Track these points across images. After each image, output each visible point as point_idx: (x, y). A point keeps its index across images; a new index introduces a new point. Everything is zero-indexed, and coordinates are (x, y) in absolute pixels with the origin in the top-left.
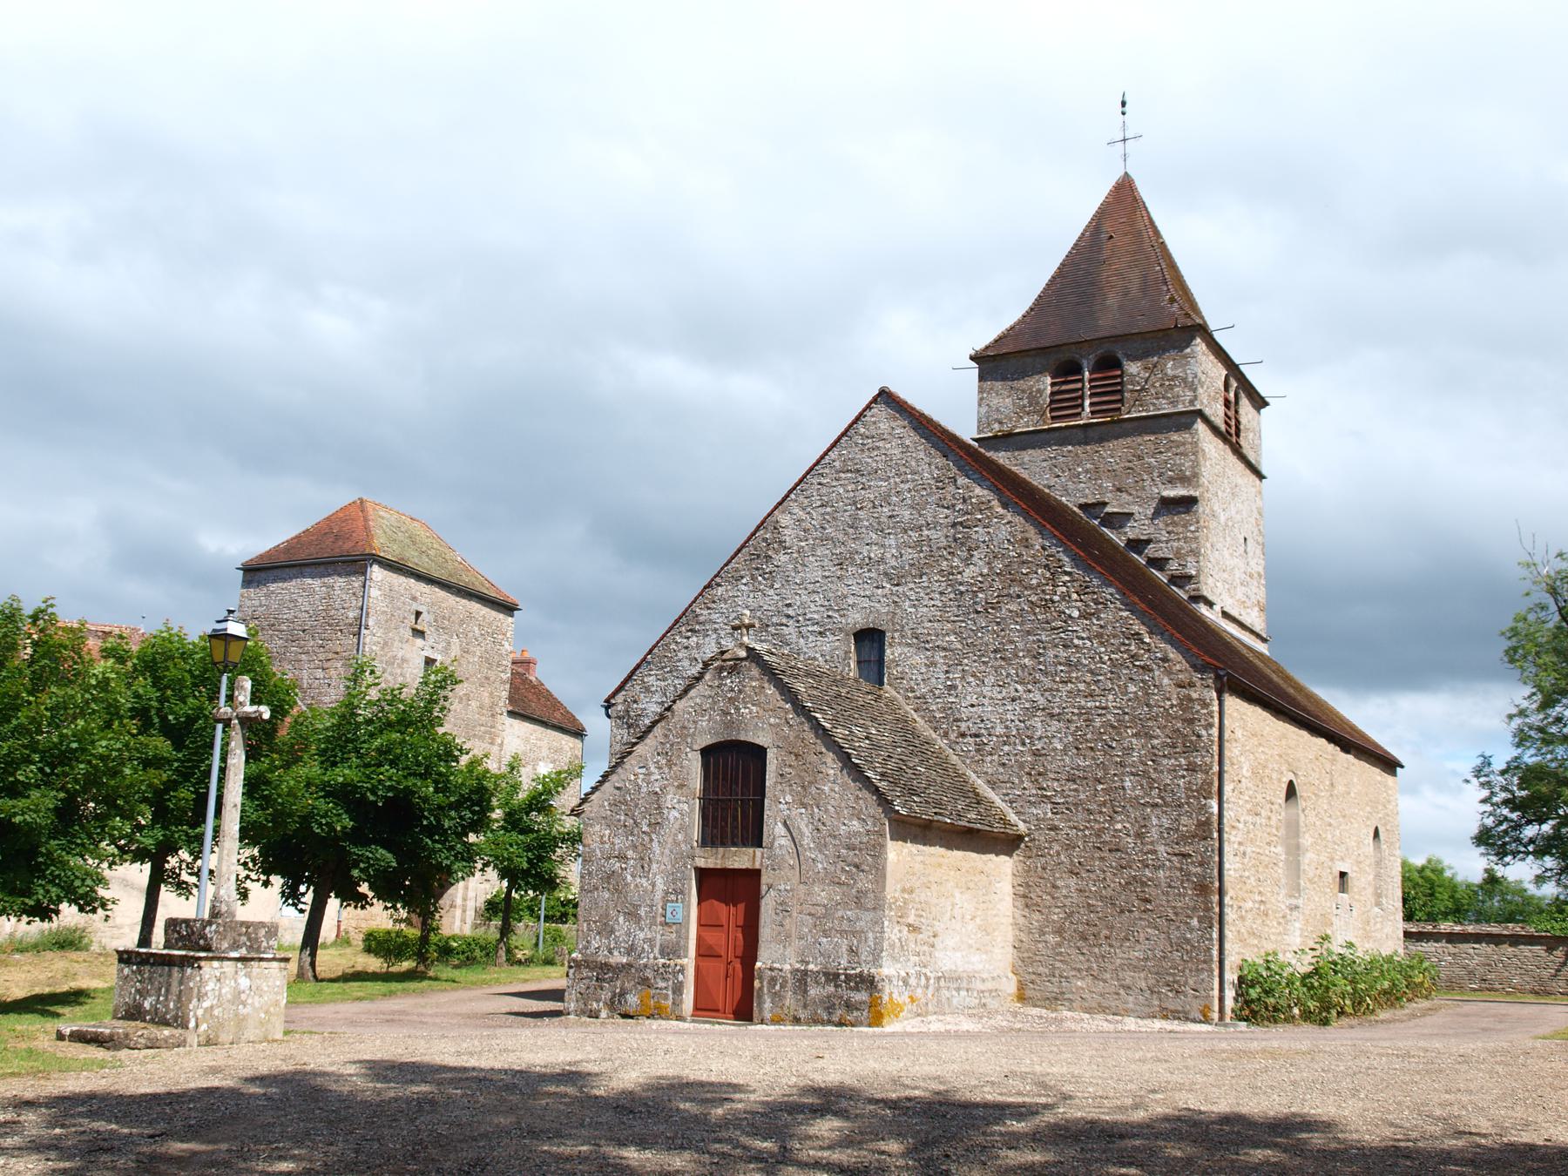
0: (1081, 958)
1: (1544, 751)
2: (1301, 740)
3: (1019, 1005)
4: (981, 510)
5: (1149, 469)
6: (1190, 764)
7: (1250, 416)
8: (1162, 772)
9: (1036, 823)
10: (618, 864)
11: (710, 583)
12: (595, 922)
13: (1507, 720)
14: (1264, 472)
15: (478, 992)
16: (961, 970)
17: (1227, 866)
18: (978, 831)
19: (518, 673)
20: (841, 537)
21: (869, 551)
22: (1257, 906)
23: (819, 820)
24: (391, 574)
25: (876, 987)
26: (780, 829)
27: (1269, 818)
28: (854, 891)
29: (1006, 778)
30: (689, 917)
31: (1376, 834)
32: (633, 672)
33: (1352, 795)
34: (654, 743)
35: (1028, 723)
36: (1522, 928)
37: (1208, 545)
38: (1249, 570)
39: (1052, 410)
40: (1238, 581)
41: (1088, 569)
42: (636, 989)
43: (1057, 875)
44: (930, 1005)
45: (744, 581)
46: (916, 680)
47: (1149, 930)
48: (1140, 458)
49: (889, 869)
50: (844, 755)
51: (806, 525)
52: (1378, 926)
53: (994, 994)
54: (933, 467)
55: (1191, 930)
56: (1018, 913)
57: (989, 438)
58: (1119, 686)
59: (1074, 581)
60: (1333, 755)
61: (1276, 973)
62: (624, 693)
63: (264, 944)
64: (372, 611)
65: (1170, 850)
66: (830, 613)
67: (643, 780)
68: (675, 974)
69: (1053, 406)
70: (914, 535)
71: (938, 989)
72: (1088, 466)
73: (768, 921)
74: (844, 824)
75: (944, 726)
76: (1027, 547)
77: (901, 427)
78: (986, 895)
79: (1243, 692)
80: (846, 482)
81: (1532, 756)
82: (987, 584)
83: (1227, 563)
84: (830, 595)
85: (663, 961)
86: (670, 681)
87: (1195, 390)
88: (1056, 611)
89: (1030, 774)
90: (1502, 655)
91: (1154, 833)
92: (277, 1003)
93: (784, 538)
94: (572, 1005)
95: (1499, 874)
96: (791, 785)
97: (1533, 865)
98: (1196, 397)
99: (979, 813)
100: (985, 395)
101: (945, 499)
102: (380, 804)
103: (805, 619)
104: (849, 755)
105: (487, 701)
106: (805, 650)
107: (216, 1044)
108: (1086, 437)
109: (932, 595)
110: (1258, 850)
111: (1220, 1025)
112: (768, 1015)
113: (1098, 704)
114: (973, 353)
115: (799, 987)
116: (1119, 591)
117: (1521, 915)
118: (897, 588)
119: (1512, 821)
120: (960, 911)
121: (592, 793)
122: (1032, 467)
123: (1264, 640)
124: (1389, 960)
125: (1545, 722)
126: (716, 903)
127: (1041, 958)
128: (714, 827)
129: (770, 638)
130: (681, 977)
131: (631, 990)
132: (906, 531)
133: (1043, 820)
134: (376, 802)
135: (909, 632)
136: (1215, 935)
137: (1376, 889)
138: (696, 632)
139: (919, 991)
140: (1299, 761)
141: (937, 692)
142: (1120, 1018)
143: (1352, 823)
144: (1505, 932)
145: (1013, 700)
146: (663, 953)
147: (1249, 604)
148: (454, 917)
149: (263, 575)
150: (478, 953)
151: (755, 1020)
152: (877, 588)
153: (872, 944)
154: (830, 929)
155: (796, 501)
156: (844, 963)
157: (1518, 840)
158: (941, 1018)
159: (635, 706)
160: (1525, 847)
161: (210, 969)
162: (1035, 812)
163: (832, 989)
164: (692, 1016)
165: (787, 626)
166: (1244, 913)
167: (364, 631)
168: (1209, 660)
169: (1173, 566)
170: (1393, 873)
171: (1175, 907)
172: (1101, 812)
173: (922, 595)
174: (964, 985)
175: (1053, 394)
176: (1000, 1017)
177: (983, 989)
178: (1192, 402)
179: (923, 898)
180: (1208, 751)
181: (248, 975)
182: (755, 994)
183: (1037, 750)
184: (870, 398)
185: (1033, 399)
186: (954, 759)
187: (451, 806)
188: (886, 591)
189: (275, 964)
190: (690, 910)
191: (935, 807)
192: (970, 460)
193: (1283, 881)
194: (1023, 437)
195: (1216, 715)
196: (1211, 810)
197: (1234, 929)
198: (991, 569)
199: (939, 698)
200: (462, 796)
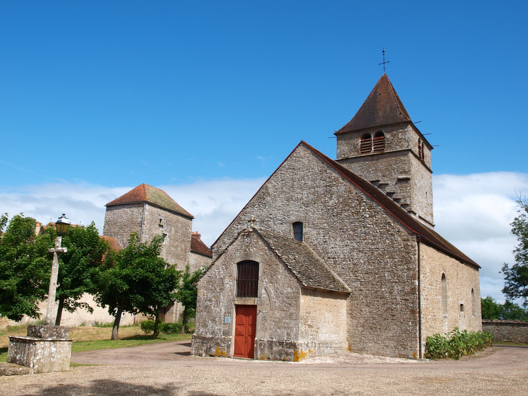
0: (371, 336)
1: (525, 262)
2: (447, 259)
3: (349, 352)
4: (335, 181)
6: (408, 268)
7: (427, 152)
8: (398, 271)
9: (354, 288)
10: (209, 303)
11: (245, 207)
12: (201, 323)
13: (513, 252)
14: (432, 171)
15: (171, 344)
16: (328, 340)
17: (421, 303)
18: (334, 291)
20: (288, 191)
22: (432, 317)
23: (277, 288)
24: (152, 207)
25: (296, 347)
26: (263, 291)
27: (436, 286)
28: (289, 313)
32: (220, 237)
33: (464, 278)
34: (221, 261)
35: (351, 254)
36: (521, 321)
37: (414, 194)
38: (428, 203)
39: (361, 150)
40: (424, 206)
41: (372, 200)
42: (215, 346)
44: (316, 353)
45: (256, 206)
46: (313, 239)
47: (394, 326)
48: (390, 165)
49: (301, 305)
52: (474, 322)
53: (340, 348)
54: (319, 167)
55: (409, 326)
56: (349, 320)
58: (383, 241)
62: (217, 244)
63: (63, 335)
64: (145, 219)
65: (401, 298)
66: (284, 217)
67: (218, 274)
68: (228, 341)
69: (362, 149)
70: (313, 190)
71: (319, 347)
73: (259, 323)
79: (426, 242)
80: (290, 172)
81: (521, 264)
82: (337, 206)
87: (408, 143)
88: (361, 215)
89: (352, 271)
90: (511, 231)
91: (396, 292)
93: (269, 192)
94: (193, 351)
96: (267, 276)
97: (522, 299)
98: (409, 145)
99: (334, 285)
104: (287, 265)
106: (276, 229)
107: (41, 373)
108: (372, 159)
112: (259, 357)
113: (375, 247)
116: (383, 208)
117: (517, 315)
118: (307, 208)
119: (515, 285)
122: (355, 169)
125: (526, 253)
126: (241, 316)
127: (357, 336)
128: (242, 289)
129: (265, 225)
130: (230, 343)
131: (213, 347)
132: (310, 189)
133: (357, 287)
135: (311, 223)
136: (418, 328)
137: (473, 309)
139: (312, 348)
140: (446, 266)
141: (320, 243)
142: (384, 357)
144: (515, 323)
146: (224, 334)
147: (428, 214)
148: (173, 317)
149: (112, 208)
150: (177, 329)
151: (255, 358)
152: (300, 208)
153: (295, 332)
155: (273, 179)
156: (285, 338)
157: (517, 291)
161: (41, 344)
163: (281, 348)
164: (234, 356)
165: (270, 221)
167: (143, 225)
169: (402, 201)
170: (478, 304)
171: (403, 318)
172: (377, 285)
173: (315, 210)
174: (329, 345)
175: (361, 145)
176: (341, 357)
177: (336, 347)
178: (407, 147)
181: (55, 347)
182: (255, 349)
184: (298, 144)
185: (355, 147)
186: (326, 266)
187: (162, 282)
188: (303, 209)
189: (66, 342)
190: (233, 319)
191: (318, 283)
192: (331, 164)
193: (441, 308)
195: (417, 251)
196: (415, 284)
198: (338, 201)
199: (321, 245)
200: (166, 278)
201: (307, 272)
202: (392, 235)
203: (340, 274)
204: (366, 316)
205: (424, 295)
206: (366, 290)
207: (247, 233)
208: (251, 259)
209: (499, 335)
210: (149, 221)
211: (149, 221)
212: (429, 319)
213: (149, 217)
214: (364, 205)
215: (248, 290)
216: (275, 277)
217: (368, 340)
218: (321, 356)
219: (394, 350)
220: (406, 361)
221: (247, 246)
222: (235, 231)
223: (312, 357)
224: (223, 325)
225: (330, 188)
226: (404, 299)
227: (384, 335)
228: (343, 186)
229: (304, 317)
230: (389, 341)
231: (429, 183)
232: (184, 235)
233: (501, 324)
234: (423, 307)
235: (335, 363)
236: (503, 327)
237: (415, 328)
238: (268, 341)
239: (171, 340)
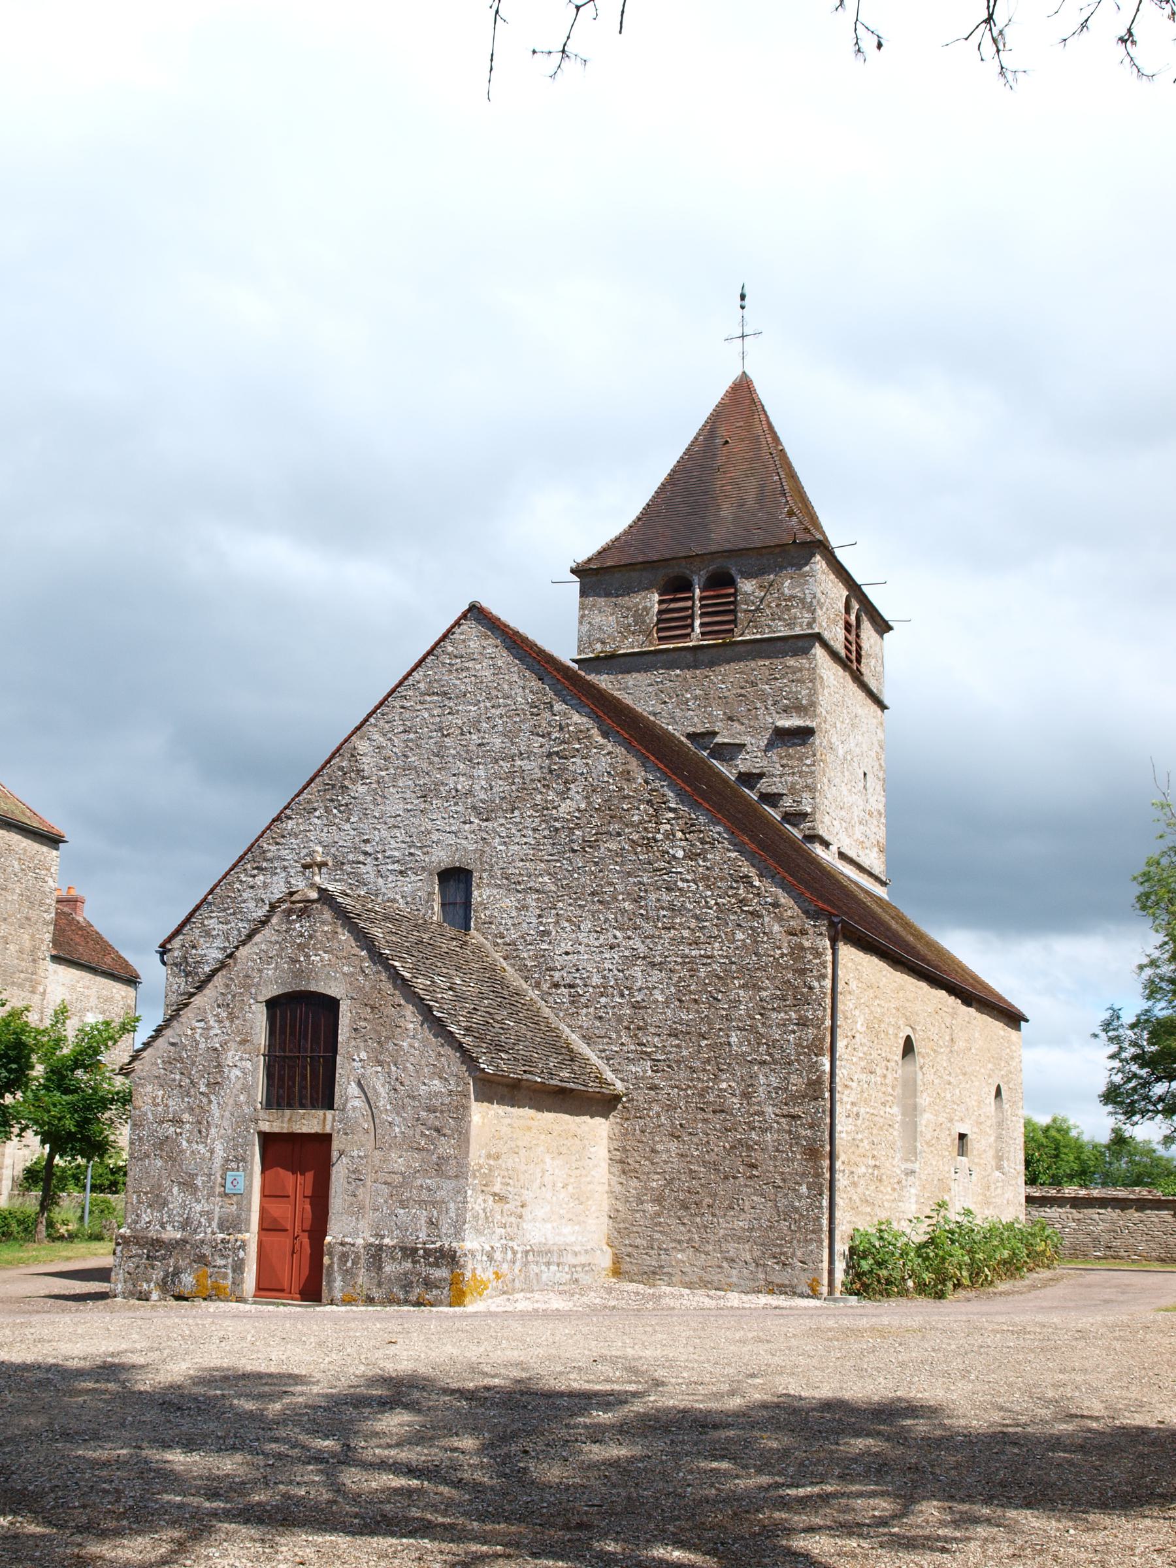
0: (682, 1228)
3: (614, 1280)
4: (579, 739)
5: (763, 697)
7: (872, 641)
8: (771, 1026)
9: (634, 1081)
10: (172, 1129)
12: (146, 1193)
14: (886, 702)
16: (551, 1242)
17: (838, 1128)
18: (572, 1090)
20: (425, 766)
22: (870, 1171)
23: (397, 1079)
25: (457, 1263)
26: (353, 1089)
27: (885, 1076)
28: (434, 1157)
29: (603, 1033)
30: (251, 1187)
32: (192, 915)
33: (973, 1051)
34: (214, 993)
36: (1150, 1192)
37: (825, 780)
38: (869, 807)
39: (659, 630)
40: (856, 819)
41: (694, 805)
42: (192, 1267)
43: (657, 1139)
45: (317, 814)
46: (506, 924)
47: (755, 1198)
48: (753, 684)
50: (425, 1008)
52: (999, 1191)
53: (587, 1268)
55: (800, 1197)
57: (590, 659)
59: (678, 818)
60: (953, 1008)
61: (889, 1243)
62: (181, 937)
65: (778, 1111)
66: (412, 850)
67: (201, 1034)
68: (235, 1250)
69: (660, 626)
70: (506, 765)
71: (526, 1264)
72: (698, 692)
74: (425, 1084)
75: (536, 975)
76: (629, 780)
77: (492, 646)
78: (580, 1160)
81: (1163, 1009)
83: (845, 800)
85: (222, 1236)
86: (233, 925)
87: (813, 612)
88: (658, 850)
89: (629, 1028)
91: (762, 1093)
93: (362, 766)
94: (120, 1286)
95: (1127, 1135)
96: (366, 1041)
98: (814, 620)
99: (573, 1072)
100: (586, 612)
101: (540, 727)
103: (385, 857)
104: (430, 1008)
105: (28, 944)
106: (384, 890)
110: (872, 1111)
111: (829, 1300)
112: (338, 1295)
113: (702, 952)
114: (574, 565)
116: (727, 830)
118: (486, 823)
119: (1141, 1078)
120: (551, 1177)
121: (143, 1050)
123: (883, 884)
126: (281, 1170)
128: (281, 1087)
129: (346, 877)
130: (241, 1254)
132: (497, 761)
133: (643, 1078)
135: (499, 872)
136: (825, 1203)
137: (997, 1151)
138: (262, 869)
139: (505, 1266)
140: (918, 1015)
141: (528, 938)
142: (723, 1293)
144: (1132, 1197)
147: (867, 844)
150: (15, 1228)
151: (324, 1300)
152: (464, 823)
153: (453, 1215)
155: (376, 726)
156: (423, 1236)
157: (1147, 1098)
158: (528, 1295)
159: (194, 951)
160: (1154, 1105)
163: (409, 1265)
164: (255, 1296)
165: (365, 864)
166: (856, 1179)
169: (787, 802)
170: (1016, 1135)
171: (782, 1173)
172: (704, 1070)
173: (513, 831)
174: (555, 1259)
175: (660, 612)
176: (592, 1294)
178: (810, 625)
179: (510, 1164)
184: (459, 614)
185: (639, 617)
186: (546, 1012)
188: (474, 827)
191: (524, 1065)
193: (899, 1144)
194: (628, 659)
195: (829, 965)
197: (845, 1196)
198: (589, 804)
201: (490, 1028)
202: (755, 914)
203: (591, 1038)
204: (668, 1168)
205: (847, 1103)
206: (672, 1087)
207: (301, 905)
212: (859, 1177)
214: (669, 820)
216: (390, 1046)
217: (675, 1241)
219: (754, 1270)
220: (789, 1303)
221: (299, 945)
222: (245, 895)
223: (504, 1293)
224: (218, 1199)
226: (787, 1116)
227: (723, 1226)
228: (604, 755)
229: (481, 1168)
230: (739, 1243)
231: (876, 744)
232: (29, 899)
233: (1089, 1202)
234: (841, 1139)
235: (575, 1309)
236: (1092, 1213)
237: (818, 1204)
239: (9, 1262)
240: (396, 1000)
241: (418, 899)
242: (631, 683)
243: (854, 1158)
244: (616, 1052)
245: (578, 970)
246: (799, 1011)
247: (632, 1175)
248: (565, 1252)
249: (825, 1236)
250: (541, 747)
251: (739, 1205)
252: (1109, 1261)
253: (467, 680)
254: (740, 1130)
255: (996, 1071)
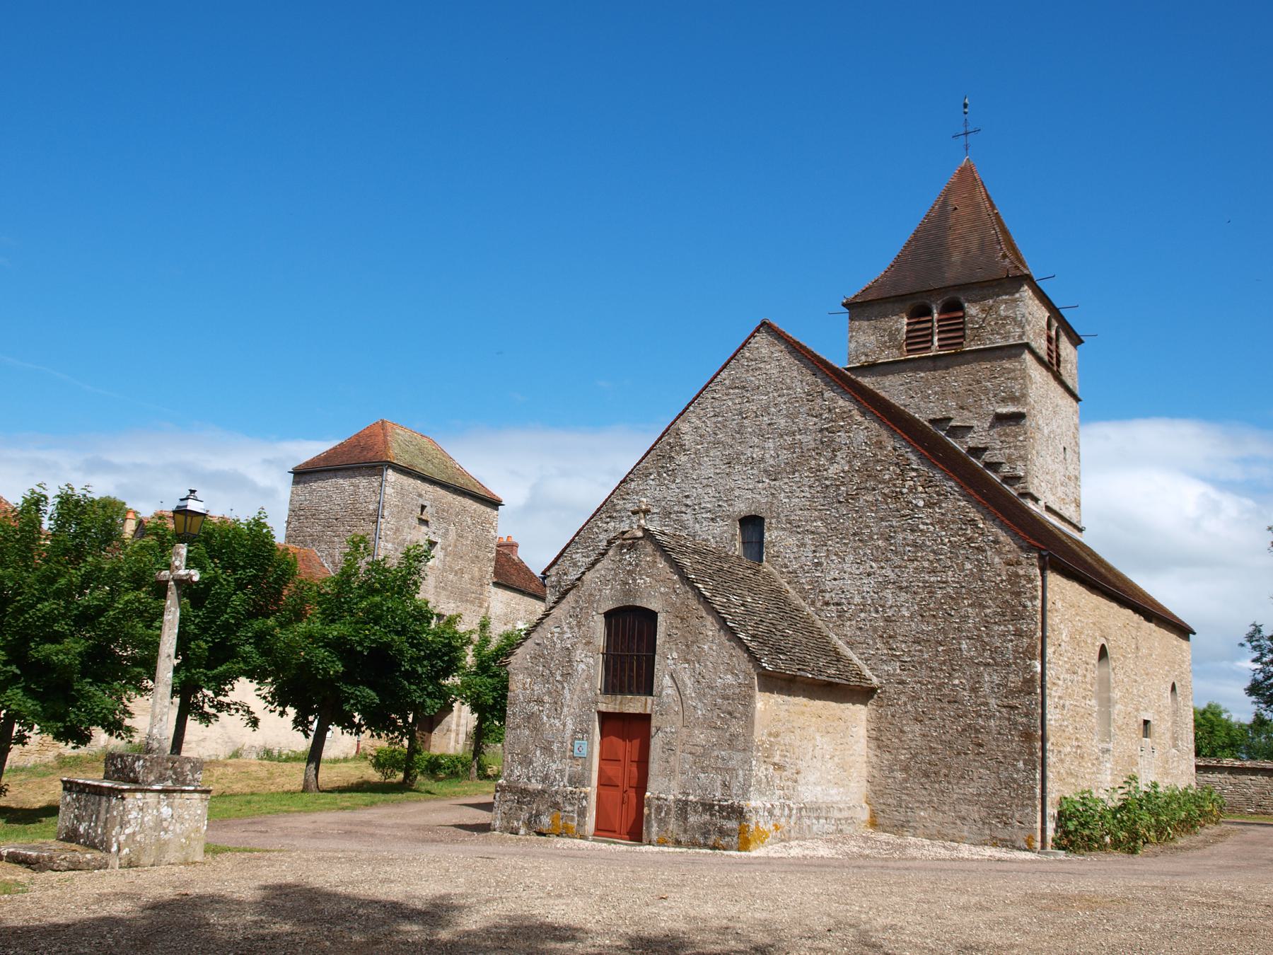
0: (924, 792)
3: (872, 830)
5: (986, 391)
7: (1068, 351)
8: (993, 636)
9: (887, 677)
10: (536, 707)
11: (625, 478)
12: (517, 754)
15: (446, 803)
17: (1048, 717)
19: (504, 554)
20: (729, 441)
21: (752, 453)
22: (1074, 750)
23: (700, 674)
24: (402, 476)
25: (744, 817)
26: (667, 681)
27: (1085, 676)
28: (728, 734)
31: (1173, 688)
32: (564, 550)
33: (1154, 656)
34: (567, 607)
37: (1034, 452)
38: (1068, 474)
39: (908, 345)
41: (932, 466)
42: (549, 811)
43: (904, 722)
44: (792, 831)
45: (652, 477)
46: (789, 557)
47: (982, 770)
48: (978, 382)
49: (757, 715)
50: (721, 620)
51: (702, 432)
52: (1175, 764)
54: (804, 384)
55: (1018, 771)
58: (957, 564)
60: (1138, 624)
61: (1091, 808)
62: (556, 567)
63: (190, 777)
65: (999, 703)
66: (720, 503)
67: (558, 638)
68: (580, 800)
69: (909, 341)
70: (789, 439)
71: (800, 818)
72: (937, 389)
73: (656, 758)
75: (812, 596)
76: (881, 448)
80: (734, 397)
82: (848, 479)
84: (721, 488)
87: (1023, 327)
89: (882, 637)
91: (986, 688)
92: (198, 830)
94: (498, 822)
96: (677, 644)
98: (1024, 333)
99: (838, 669)
101: (814, 409)
102: (366, 654)
104: (725, 620)
105: (477, 574)
106: (700, 533)
107: (137, 867)
108: (934, 366)
109: (803, 488)
110: (1075, 703)
111: (1042, 854)
112: (655, 838)
113: (939, 579)
115: (681, 815)
116: (958, 484)
122: (892, 389)
124: (1185, 793)
127: (891, 792)
129: (672, 523)
130: (584, 803)
131: (545, 813)
132: (782, 436)
133: (893, 675)
134: (362, 652)
135: (784, 519)
136: (1038, 776)
137: (1173, 733)
139: (783, 820)
140: (1110, 628)
141: (806, 568)
142: (956, 844)
143: (1153, 680)
145: (869, 575)
146: (571, 782)
147: (1067, 500)
148: (450, 739)
149: (308, 477)
151: (644, 841)
152: (759, 482)
153: (741, 780)
154: (707, 766)
155: (694, 412)
156: (718, 795)
158: (801, 843)
161: (133, 800)
162: (886, 669)
164: (594, 835)
165: (686, 513)
166: (1063, 756)
167: (380, 520)
168: (1033, 542)
169: (1006, 469)
171: (1003, 751)
172: (941, 670)
173: (794, 488)
174: (824, 814)
175: (908, 332)
178: (1020, 337)
179: (787, 741)
180: (1032, 619)
181: (170, 805)
182: (645, 819)
183: (889, 616)
185: (893, 336)
186: (819, 623)
188: (766, 485)
189: (196, 795)
191: (798, 664)
192: (834, 378)
195: (1040, 589)
196: (1035, 669)
198: (851, 466)
199: (808, 572)
204: (913, 745)
205: (1055, 697)
206: (916, 682)
208: (638, 604)
209: (1237, 798)
210: (395, 510)
211: (395, 510)
212: (1065, 755)
213: (395, 501)
215: (631, 677)
216: (695, 648)
217: (919, 801)
218: (805, 839)
219: (981, 827)
220: (1009, 855)
221: (628, 571)
222: (601, 537)
223: (782, 841)
224: (568, 760)
225: (830, 435)
228: (862, 430)
229: (763, 743)
232: (479, 544)
234: (1051, 725)
235: (836, 856)
236: (1245, 778)
237: (1032, 777)
238: (677, 801)
239: (445, 795)
240: (699, 613)
241: (724, 539)
242: (887, 384)
243: (1061, 740)
244: (873, 655)
245: (843, 592)
246: (1015, 624)
247: (885, 749)
248: (831, 809)
249: (1038, 803)
250: (815, 425)
251: (969, 775)
252: (1260, 816)
253: (759, 377)
254: (970, 717)
255: (1172, 672)
